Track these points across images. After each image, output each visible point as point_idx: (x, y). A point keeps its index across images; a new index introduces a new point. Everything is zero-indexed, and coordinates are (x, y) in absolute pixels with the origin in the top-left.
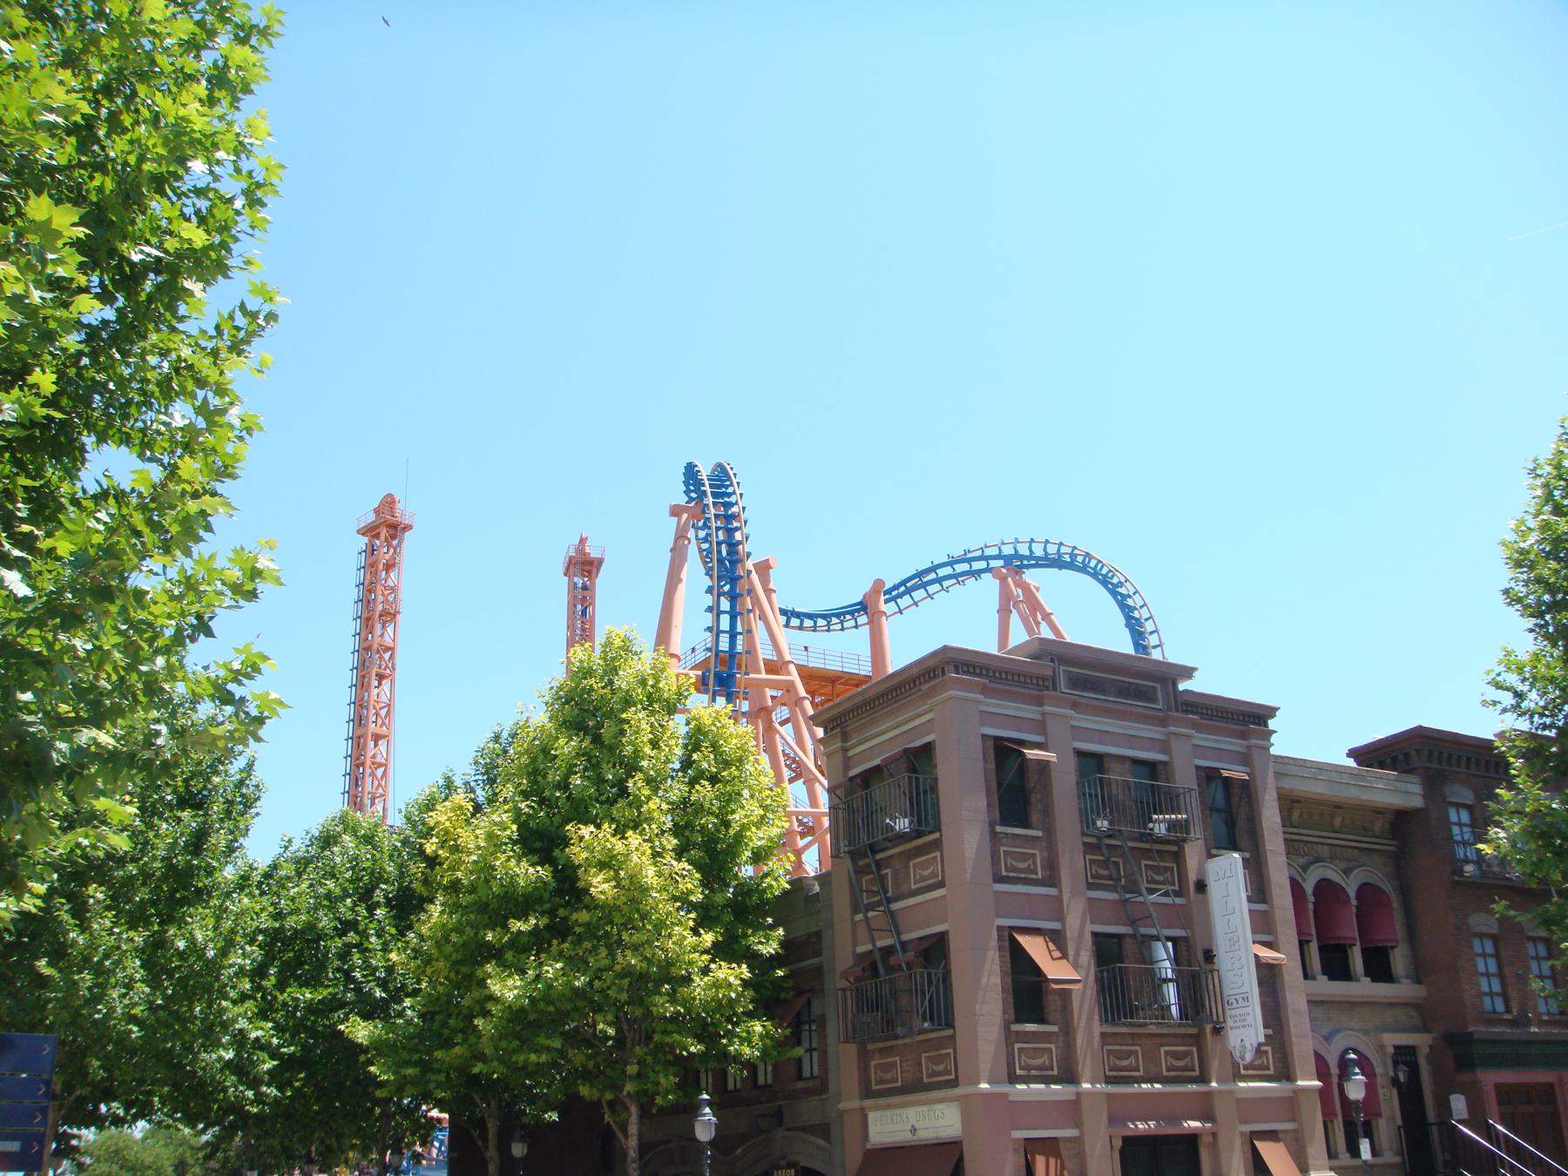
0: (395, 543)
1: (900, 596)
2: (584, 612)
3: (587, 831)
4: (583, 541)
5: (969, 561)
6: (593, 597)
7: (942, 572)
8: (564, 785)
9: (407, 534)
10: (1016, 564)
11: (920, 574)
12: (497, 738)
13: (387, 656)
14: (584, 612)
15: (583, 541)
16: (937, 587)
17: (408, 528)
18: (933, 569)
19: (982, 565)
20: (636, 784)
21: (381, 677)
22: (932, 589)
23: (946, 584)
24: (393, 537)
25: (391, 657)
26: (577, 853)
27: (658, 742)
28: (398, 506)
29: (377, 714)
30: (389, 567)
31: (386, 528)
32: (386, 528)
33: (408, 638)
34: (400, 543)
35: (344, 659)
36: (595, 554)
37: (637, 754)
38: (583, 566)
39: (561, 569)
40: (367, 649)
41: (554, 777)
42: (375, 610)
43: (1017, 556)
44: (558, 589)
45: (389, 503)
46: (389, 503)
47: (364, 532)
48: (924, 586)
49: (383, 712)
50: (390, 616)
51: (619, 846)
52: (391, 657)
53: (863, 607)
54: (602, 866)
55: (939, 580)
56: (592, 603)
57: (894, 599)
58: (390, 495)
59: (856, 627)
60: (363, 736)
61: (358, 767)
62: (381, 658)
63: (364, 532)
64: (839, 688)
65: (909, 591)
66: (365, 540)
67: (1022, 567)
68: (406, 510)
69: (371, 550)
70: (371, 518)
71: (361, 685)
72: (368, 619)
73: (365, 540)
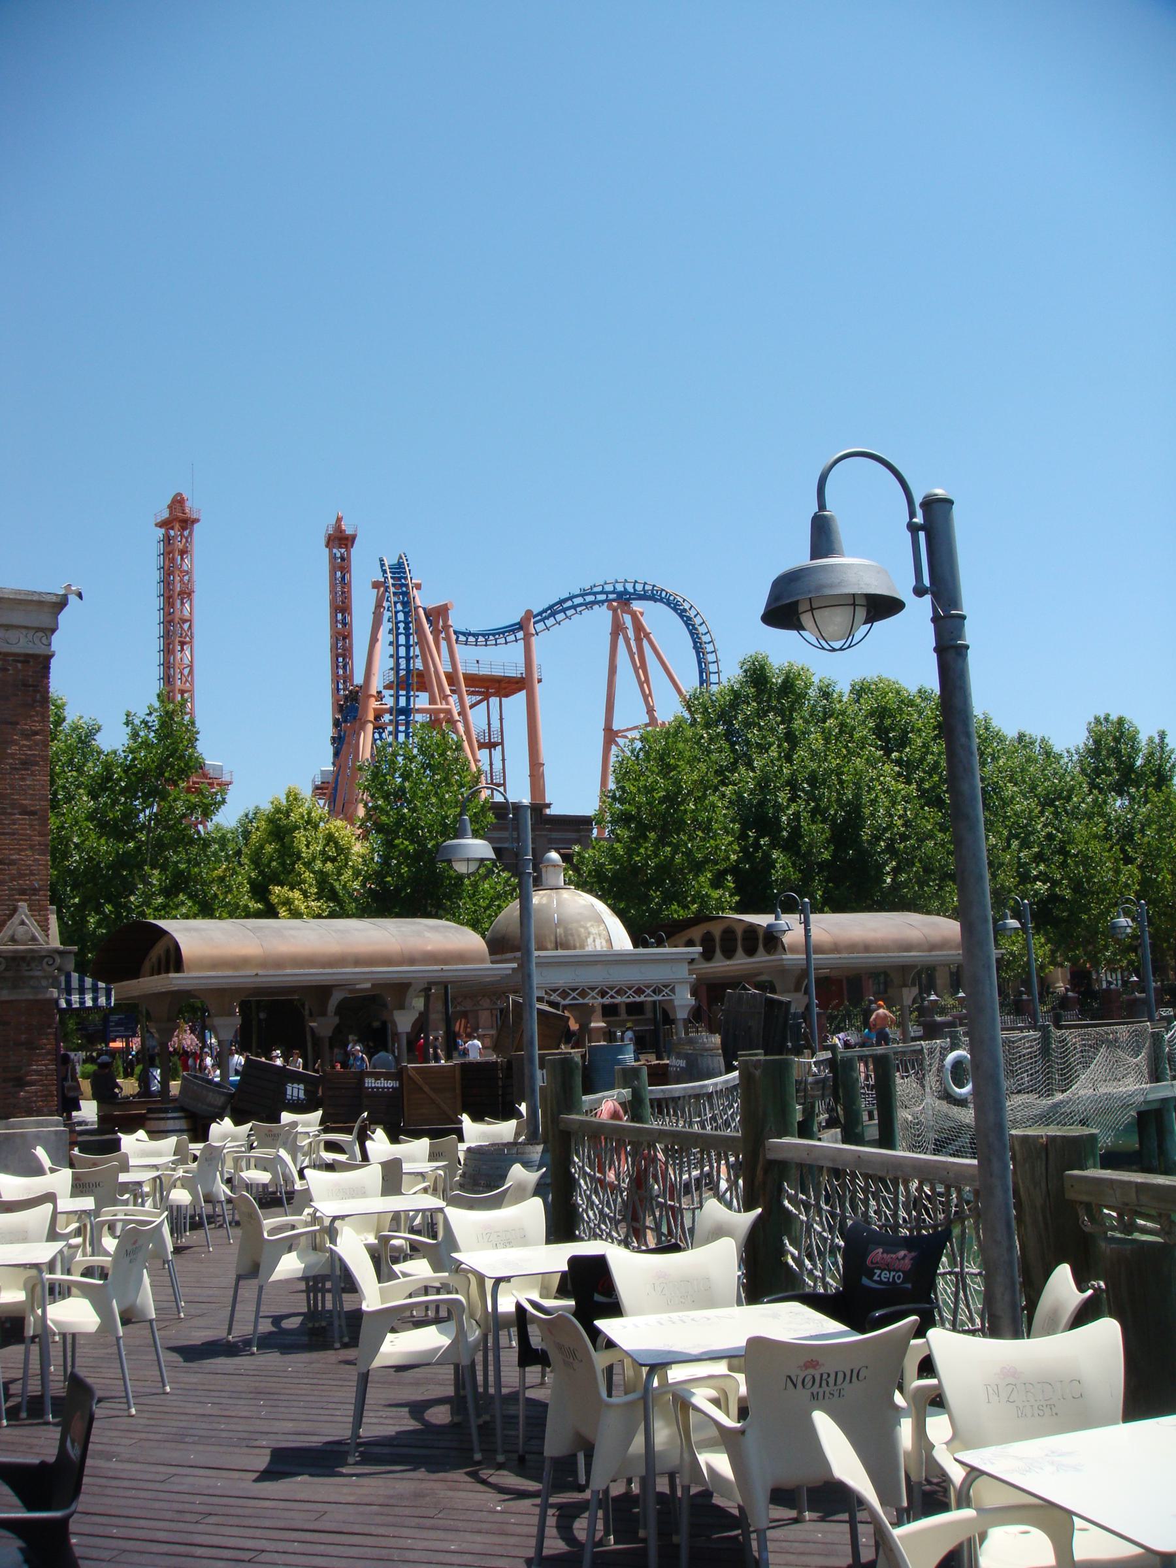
0: (186, 533)
1: (547, 618)
2: (343, 578)
3: (277, 889)
4: (339, 520)
5: (595, 594)
6: (349, 566)
7: (578, 601)
8: (269, 866)
9: (196, 526)
10: (623, 599)
11: (562, 602)
12: (247, 816)
13: (186, 626)
14: (343, 578)
15: (339, 520)
16: (573, 611)
17: (197, 521)
18: (571, 598)
19: (603, 597)
20: (299, 867)
21: (182, 644)
22: (569, 613)
23: (579, 609)
24: (184, 529)
25: (190, 627)
26: (274, 900)
27: (306, 844)
28: (188, 504)
29: (182, 674)
30: (183, 552)
31: (178, 521)
32: (178, 521)
33: (204, 611)
34: (191, 534)
35: (153, 630)
36: (349, 531)
37: (300, 852)
38: (340, 540)
39: (323, 542)
40: (169, 622)
41: (265, 861)
42: (174, 591)
43: (626, 592)
44: (322, 558)
45: (178, 502)
46: (178, 502)
47: (161, 525)
48: (564, 611)
49: (186, 671)
50: (187, 594)
51: (291, 894)
52: (190, 627)
53: (520, 626)
54: (284, 904)
55: (574, 607)
56: (349, 571)
57: (543, 620)
58: (179, 494)
59: (516, 641)
60: (173, 691)
61: (169, 575)
62: (182, 628)
63: (161, 525)
64: (503, 685)
65: (553, 615)
66: (163, 531)
67: (629, 599)
68: (193, 506)
69: (167, 540)
70: (166, 514)
71: (168, 651)
72: (169, 597)
73: (163, 531)
